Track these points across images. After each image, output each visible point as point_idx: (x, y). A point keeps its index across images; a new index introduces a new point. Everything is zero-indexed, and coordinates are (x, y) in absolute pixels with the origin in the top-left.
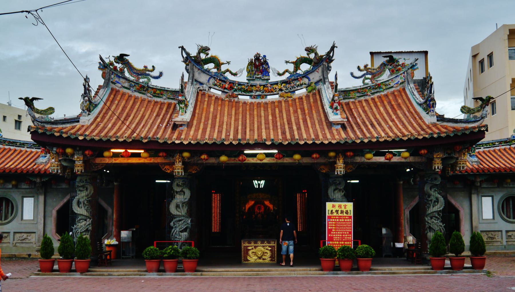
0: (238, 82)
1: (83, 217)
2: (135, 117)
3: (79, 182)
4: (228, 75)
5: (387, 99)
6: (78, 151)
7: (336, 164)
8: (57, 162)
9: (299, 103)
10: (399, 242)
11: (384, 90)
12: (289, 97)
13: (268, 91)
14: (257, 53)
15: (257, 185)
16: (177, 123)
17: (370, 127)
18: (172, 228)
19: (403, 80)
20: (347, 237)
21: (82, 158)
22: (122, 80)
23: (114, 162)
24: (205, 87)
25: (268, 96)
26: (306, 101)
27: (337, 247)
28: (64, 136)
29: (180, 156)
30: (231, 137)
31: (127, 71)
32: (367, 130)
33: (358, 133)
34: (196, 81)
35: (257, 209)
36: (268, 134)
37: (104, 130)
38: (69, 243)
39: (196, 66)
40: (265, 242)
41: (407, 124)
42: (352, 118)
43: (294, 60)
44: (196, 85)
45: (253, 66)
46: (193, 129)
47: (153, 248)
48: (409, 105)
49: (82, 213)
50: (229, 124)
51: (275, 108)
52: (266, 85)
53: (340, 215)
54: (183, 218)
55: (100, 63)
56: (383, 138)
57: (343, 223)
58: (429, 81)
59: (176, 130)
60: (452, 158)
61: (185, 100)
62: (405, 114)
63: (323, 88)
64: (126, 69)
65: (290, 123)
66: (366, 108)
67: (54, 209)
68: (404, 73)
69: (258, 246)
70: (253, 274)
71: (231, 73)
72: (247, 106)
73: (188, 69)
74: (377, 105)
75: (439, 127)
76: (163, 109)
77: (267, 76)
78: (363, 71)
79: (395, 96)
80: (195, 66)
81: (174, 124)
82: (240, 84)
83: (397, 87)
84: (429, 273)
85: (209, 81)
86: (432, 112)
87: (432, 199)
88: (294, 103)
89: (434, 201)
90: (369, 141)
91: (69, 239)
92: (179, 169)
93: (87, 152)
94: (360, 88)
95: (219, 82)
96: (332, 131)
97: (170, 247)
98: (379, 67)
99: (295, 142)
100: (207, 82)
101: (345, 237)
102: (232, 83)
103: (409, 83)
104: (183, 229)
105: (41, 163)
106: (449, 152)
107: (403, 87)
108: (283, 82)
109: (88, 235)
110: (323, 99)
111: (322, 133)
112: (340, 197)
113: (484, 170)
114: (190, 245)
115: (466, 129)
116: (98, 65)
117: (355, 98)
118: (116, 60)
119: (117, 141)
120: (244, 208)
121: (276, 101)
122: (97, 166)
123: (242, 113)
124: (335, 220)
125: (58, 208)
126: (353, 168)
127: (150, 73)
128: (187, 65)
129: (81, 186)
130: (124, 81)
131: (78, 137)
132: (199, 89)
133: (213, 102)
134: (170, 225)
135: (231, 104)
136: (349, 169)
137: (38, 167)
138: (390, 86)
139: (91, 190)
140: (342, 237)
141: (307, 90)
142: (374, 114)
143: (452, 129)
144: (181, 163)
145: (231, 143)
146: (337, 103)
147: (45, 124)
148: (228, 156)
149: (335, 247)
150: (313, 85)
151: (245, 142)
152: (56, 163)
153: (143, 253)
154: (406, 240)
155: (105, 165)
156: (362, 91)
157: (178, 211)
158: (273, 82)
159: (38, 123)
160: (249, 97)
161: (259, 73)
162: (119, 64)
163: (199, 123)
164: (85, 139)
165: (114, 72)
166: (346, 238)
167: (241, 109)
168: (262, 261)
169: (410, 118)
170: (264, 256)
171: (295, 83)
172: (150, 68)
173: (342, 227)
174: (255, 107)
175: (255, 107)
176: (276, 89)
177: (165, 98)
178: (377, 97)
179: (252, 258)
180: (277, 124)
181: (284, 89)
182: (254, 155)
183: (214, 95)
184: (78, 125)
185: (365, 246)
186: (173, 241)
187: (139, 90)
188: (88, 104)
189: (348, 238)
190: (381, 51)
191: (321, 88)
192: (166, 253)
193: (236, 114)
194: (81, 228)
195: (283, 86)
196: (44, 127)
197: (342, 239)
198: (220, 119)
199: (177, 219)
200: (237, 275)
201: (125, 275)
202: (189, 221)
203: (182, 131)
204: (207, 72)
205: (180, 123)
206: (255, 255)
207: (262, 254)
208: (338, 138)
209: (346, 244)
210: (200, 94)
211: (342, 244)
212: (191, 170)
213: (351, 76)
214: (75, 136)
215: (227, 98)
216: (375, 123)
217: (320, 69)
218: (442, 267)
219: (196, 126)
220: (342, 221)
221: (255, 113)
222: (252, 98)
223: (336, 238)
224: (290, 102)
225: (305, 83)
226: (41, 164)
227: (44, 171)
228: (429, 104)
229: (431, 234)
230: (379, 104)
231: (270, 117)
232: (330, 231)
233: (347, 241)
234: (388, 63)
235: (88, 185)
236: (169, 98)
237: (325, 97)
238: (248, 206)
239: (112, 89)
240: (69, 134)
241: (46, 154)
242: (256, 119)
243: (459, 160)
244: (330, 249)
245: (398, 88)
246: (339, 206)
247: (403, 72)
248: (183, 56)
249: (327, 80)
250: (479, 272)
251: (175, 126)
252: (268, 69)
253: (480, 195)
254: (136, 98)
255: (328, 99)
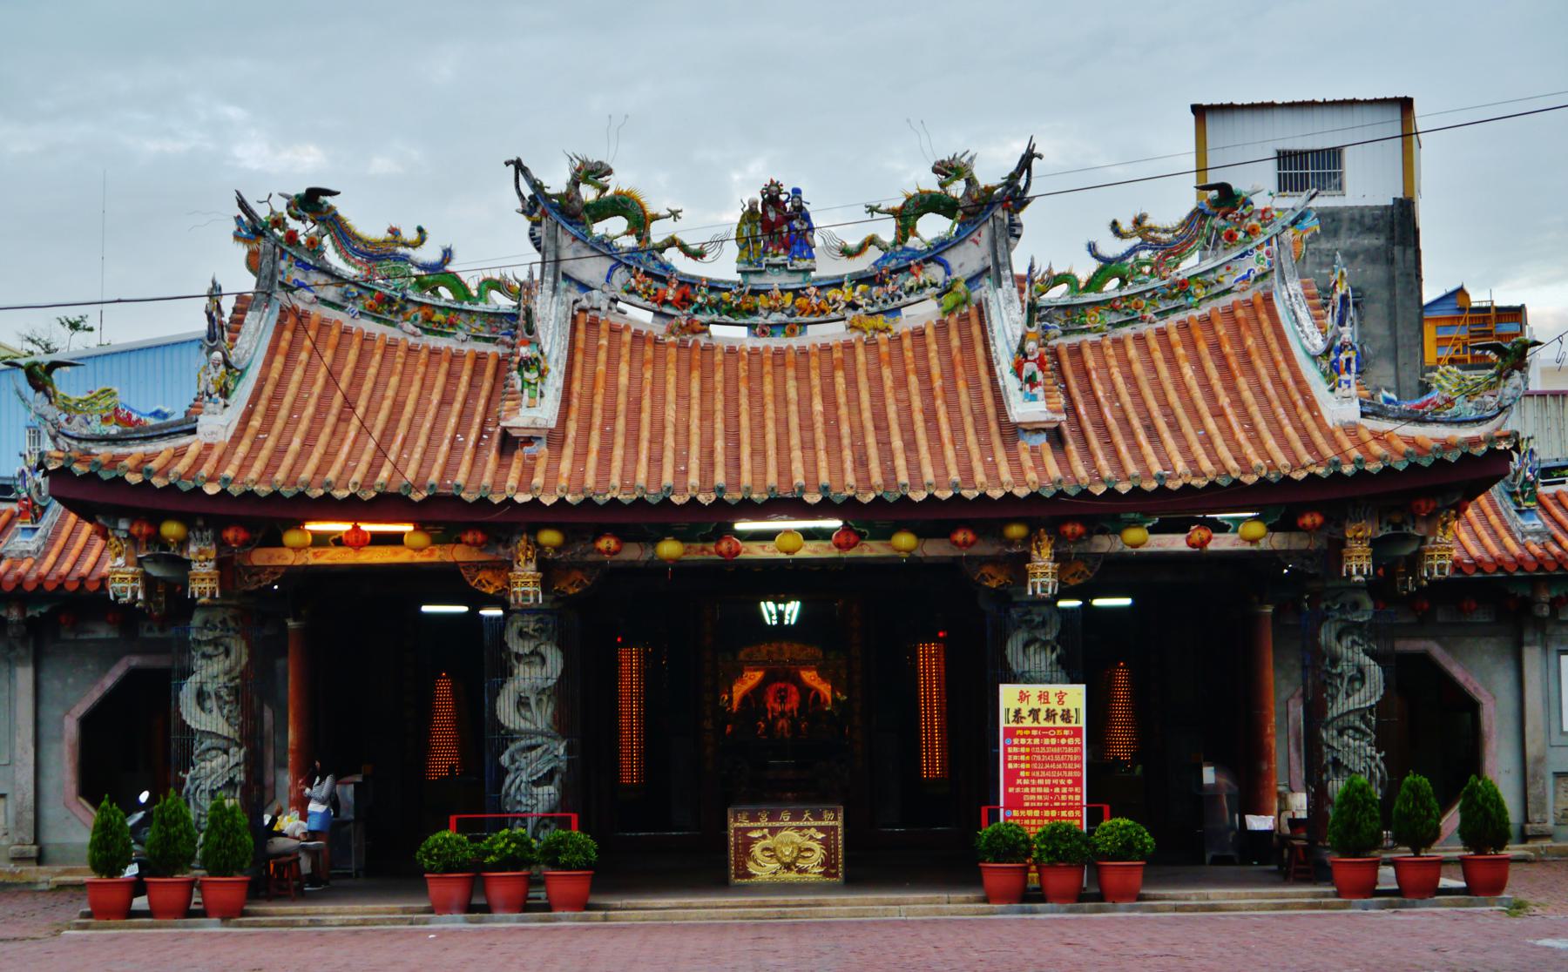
0: (709, 280)
1: (215, 742)
2: (371, 409)
3: (200, 629)
4: (673, 256)
5: (1209, 334)
6: (201, 530)
7: (1029, 562)
8: (132, 565)
9: (914, 351)
10: (1260, 811)
11: (1200, 300)
12: (882, 331)
13: (809, 310)
14: (772, 181)
15: (775, 617)
16: (515, 433)
17: (1142, 437)
18: (506, 772)
19: (1267, 267)
20: (1068, 794)
21: (212, 551)
22: (315, 277)
23: (312, 561)
24: (598, 298)
25: (809, 327)
26: (937, 343)
27: (1037, 826)
28: (159, 482)
29: (528, 544)
30: (694, 479)
31: (333, 244)
32: (1129, 448)
33: (1102, 462)
34: (566, 277)
35: (775, 700)
36: (811, 467)
37: (281, 459)
38: (182, 824)
39: (567, 226)
40: (806, 816)
41: (1262, 425)
42: (1086, 404)
43: (898, 204)
44: (567, 291)
45: (759, 224)
46: (568, 451)
47: (451, 838)
48: (1279, 357)
49: (214, 730)
50: (682, 430)
51: (834, 368)
52: (804, 289)
53: (1044, 724)
54: (539, 740)
55: (238, 218)
56: (1180, 477)
57: (1054, 750)
58: (1336, 283)
59: (512, 455)
60: (1408, 538)
61: (540, 357)
62: (1263, 391)
63: (994, 300)
64: (327, 240)
65: (883, 425)
66: (1138, 368)
67: (67, 713)
68: (1269, 242)
69: (781, 828)
70: (768, 913)
71: (683, 248)
72: (741, 364)
73: (540, 238)
74: (1173, 353)
75: (1366, 436)
76: (459, 378)
77: (805, 258)
78: (1131, 237)
79: (1236, 322)
80: (563, 227)
81: (505, 433)
82: (714, 287)
83: (1243, 290)
84: (1326, 907)
85: (609, 277)
86: (1344, 385)
87: (1343, 670)
88: (895, 352)
89: (1352, 676)
90: (1134, 487)
91: (181, 812)
92: (526, 584)
93: (230, 534)
94: (1121, 297)
95: (644, 282)
96: (1018, 455)
97: (506, 831)
98: (1182, 224)
99: (898, 495)
100: (603, 280)
101: (1060, 794)
102: (689, 283)
103: (1283, 279)
104: (540, 774)
105: (24, 555)
106: (1397, 519)
107: (1265, 291)
108: (860, 279)
109: (234, 797)
110: (993, 339)
111: (985, 463)
112: (1043, 669)
113: (1561, 562)
114: (564, 824)
115: (1447, 446)
116: (233, 227)
117: (1102, 331)
118: (292, 209)
119: (327, 497)
120: (726, 698)
121: (837, 346)
122: (257, 574)
123: (725, 388)
124: (1030, 740)
125: (81, 709)
126: (1088, 572)
127: (409, 251)
128: (536, 224)
129: (208, 643)
130: (322, 279)
131: (201, 488)
132: (577, 305)
133: (625, 351)
134: (499, 764)
135: (685, 354)
136: (1073, 575)
137: (10, 568)
138: (1222, 289)
139: (240, 652)
140: (1052, 794)
141: (940, 305)
142: (1162, 389)
143: (1404, 447)
144: (532, 566)
145: (693, 500)
146: (1034, 361)
147: (90, 445)
148: (680, 537)
149: (1030, 826)
150: (961, 286)
151: (739, 496)
152: (131, 569)
153: (418, 853)
154: (1284, 805)
155: (283, 570)
156: (1126, 307)
157: (525, 719)
158: (827, 278)
159: (68, 440)
160: (745, 329)
161: (779, 248)
162: (304, 222)
163: (586, 429)
164: (224, 493)
165: (290, 250)
166: (1063, 798)
167: (719, 376)
168: (797, 875)
169: (1276, 403)
170: (800, 860)
171: (900, 282)
172: (410, 234)
173: (1050, 762)
174: (768, 368)
175: (768, 368)
176: (835, 301)
177: (464, 337)
178: (1177, 327)
179: (763, 868)
180: (838, 427)
181: (862, 302)
182: (769, 536)
183: (627, 327)
184: (194, 444)
185: (1123, 822)
186: (508, 812)
187: (376, 311)
188: (222, 376)
189: (1071, 797)
190: (1235, 102)
191: (986, 299)
192: (492, 853)
193: (702, 392)
194: (213, 777)
195: (862, 293)
196: (89, 454)
197: (1051, 801)
198: (652, 415)
199: (523, 743)
200: (719, 918)
201: (364, 923)
202: (562, 751)
203: (534, 458)
204: (604, 247)
205: (526, 434)
206: (771, 856)
207: (795, 855)
208: (1036, 479)
209: (1064, 818)
210: (582, 323)
211: (1050, 818)
212: (563, 585)
213: (1088, 254)
214: (192, 484)
215: (674, 334)
216: (1161, 423)
217: (985, 231)
218: (1369, 889)
219: (576, 442)
220: (1050, 745)
221: (768, 388)
222: (755, 335)
223: (1033, 797)
224: (884, 349)
225: (934, 281)
226: (23, 559)
227: (35, 581)
228: (1337, 360)
229: (1340, 782)
230: (1180, 351)
231: (818, 406)
232: (1012, 776)
233: (1067, 808)
234: (1215, 207)
235: (232, 637)
236: (476, 338)
237: (999, 331)
238: (739, 690)
239: (284, 313)
240: (172, 479)
241: (37, 522)
242: (770, 414)
243: (1427, 547)
244: (1011, 831)
245: (1249, 295)
246: (1040, 697)
247: (1267, 237)
248: (520, 194)
249: (1008, 272)
250: (1487, 904)
251: (509, 443)
252: (809, 233)
253: (1554, 647)
254: (367, 339)
255: (1008, 343)
